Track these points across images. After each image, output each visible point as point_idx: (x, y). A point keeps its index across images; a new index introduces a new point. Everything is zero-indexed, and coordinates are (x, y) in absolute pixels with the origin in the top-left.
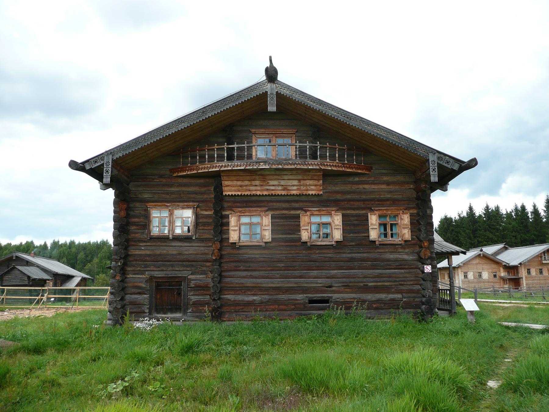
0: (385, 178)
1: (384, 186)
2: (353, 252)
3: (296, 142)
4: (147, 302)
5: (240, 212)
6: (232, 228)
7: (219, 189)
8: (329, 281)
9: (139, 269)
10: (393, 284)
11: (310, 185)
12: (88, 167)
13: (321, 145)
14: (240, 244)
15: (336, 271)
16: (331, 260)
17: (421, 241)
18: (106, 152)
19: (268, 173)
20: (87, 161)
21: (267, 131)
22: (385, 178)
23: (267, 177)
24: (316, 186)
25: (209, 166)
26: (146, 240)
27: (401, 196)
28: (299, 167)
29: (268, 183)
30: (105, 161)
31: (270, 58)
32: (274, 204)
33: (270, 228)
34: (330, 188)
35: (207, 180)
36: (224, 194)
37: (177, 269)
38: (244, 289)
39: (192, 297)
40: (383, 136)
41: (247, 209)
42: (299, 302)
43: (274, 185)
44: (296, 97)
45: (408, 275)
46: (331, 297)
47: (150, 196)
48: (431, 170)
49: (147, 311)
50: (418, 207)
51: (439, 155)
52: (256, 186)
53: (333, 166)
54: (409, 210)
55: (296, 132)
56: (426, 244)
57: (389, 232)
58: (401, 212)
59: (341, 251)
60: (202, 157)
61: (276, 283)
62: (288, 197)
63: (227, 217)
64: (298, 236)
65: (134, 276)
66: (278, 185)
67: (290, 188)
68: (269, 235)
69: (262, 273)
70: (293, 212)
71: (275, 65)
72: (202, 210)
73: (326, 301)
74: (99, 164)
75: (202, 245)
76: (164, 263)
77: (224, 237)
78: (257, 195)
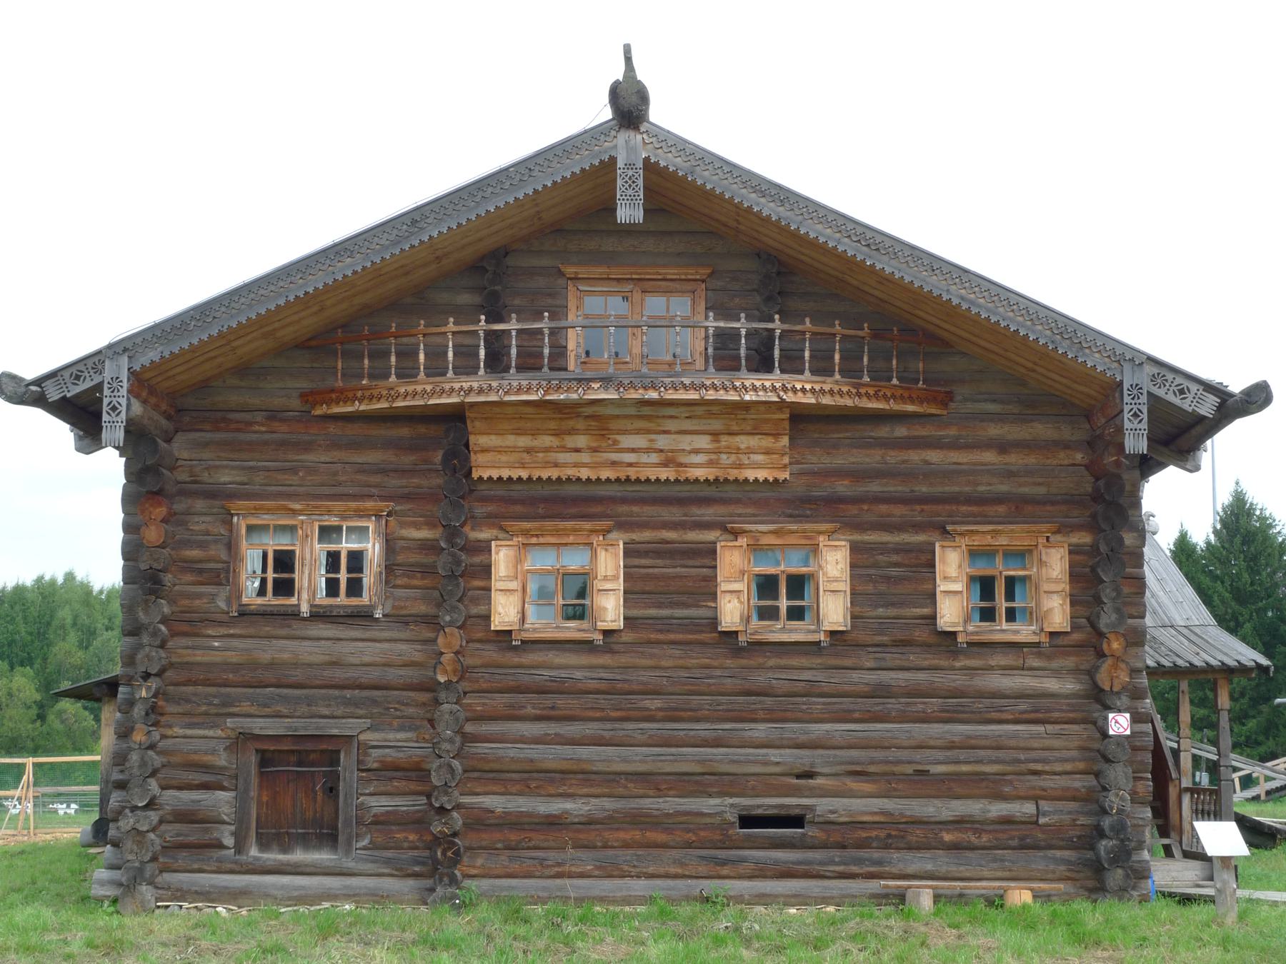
0: (994, 431)
1: (989, 457)
2: (883, 664)
3: (707, 318)
4: (226, 812)
5: (526, 533)
6: (501, 585)
7: (458, 459)
8: (803, 758)
9: (204, 708)
10: (1009, 768)
11: (750, 451)
12: (53, 395)
13: (786, 327)
14: (525, 636)
15: (827, 726)
16: (811, 691)
17: (1101, 635)
18: (110, 346)
19: (617, 412)
20: (53, 375)
21: (616, 273)
22: (994, 431)
23: (614, 425)
24: (767, 452)
25: (429, 388)
26: (224, 618)
27: (1042, 490)
28: (711, 395)
29: (616, 442)
30: (107, 375)
31: (627, 51)
32: (635, 509)
33: (620, 585)
34: (814, 459)
35: (422, 429)
36: (475, 475)
37: (326, 712)
38: (533, 778)
39: (373, 801)
40: (979, 306)
41: (549, 524)
42: (708, 820)
43: (633, 450)
44: (706, 178)
45: (1056, 743)
46: (811, 808)
47: (238, 479)
48: (1126, 415)
49: (229, 841)
50: (1093, 526)
51: (1155, 370)
52: (577, 450)
53: (822, 391)
54: (1067, 534)
55: (710, 275)
56: (1115, 645)
57: (1002, 604)
58: (1042, 541)
59: (847, 662)
60: (407, 355)
61: (638, 758)
62: (678, 488)
63: (485, 548)
64: (709, 613)
65: (189, 732)
66: (648, 450)
67: (684, 459)
68: (617, 607)
69: (591, 729)
70: (692, 536)
71: (641, 76)
72: (403, 525)
73: (796, 821)
74: (88, 384)
75: (402, 635)
76: (285, 691)
77: (474, 610)
78: (579, 479)
